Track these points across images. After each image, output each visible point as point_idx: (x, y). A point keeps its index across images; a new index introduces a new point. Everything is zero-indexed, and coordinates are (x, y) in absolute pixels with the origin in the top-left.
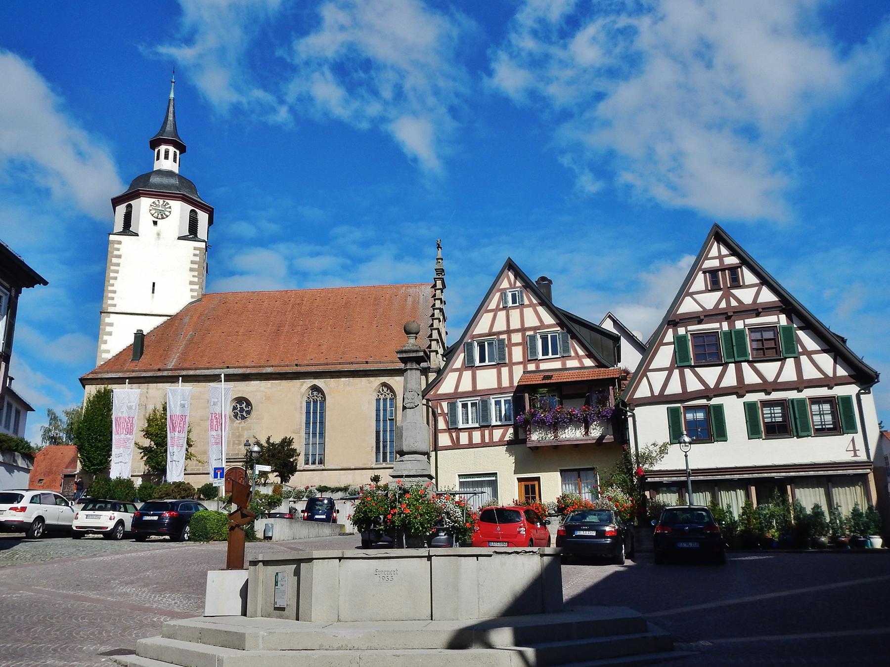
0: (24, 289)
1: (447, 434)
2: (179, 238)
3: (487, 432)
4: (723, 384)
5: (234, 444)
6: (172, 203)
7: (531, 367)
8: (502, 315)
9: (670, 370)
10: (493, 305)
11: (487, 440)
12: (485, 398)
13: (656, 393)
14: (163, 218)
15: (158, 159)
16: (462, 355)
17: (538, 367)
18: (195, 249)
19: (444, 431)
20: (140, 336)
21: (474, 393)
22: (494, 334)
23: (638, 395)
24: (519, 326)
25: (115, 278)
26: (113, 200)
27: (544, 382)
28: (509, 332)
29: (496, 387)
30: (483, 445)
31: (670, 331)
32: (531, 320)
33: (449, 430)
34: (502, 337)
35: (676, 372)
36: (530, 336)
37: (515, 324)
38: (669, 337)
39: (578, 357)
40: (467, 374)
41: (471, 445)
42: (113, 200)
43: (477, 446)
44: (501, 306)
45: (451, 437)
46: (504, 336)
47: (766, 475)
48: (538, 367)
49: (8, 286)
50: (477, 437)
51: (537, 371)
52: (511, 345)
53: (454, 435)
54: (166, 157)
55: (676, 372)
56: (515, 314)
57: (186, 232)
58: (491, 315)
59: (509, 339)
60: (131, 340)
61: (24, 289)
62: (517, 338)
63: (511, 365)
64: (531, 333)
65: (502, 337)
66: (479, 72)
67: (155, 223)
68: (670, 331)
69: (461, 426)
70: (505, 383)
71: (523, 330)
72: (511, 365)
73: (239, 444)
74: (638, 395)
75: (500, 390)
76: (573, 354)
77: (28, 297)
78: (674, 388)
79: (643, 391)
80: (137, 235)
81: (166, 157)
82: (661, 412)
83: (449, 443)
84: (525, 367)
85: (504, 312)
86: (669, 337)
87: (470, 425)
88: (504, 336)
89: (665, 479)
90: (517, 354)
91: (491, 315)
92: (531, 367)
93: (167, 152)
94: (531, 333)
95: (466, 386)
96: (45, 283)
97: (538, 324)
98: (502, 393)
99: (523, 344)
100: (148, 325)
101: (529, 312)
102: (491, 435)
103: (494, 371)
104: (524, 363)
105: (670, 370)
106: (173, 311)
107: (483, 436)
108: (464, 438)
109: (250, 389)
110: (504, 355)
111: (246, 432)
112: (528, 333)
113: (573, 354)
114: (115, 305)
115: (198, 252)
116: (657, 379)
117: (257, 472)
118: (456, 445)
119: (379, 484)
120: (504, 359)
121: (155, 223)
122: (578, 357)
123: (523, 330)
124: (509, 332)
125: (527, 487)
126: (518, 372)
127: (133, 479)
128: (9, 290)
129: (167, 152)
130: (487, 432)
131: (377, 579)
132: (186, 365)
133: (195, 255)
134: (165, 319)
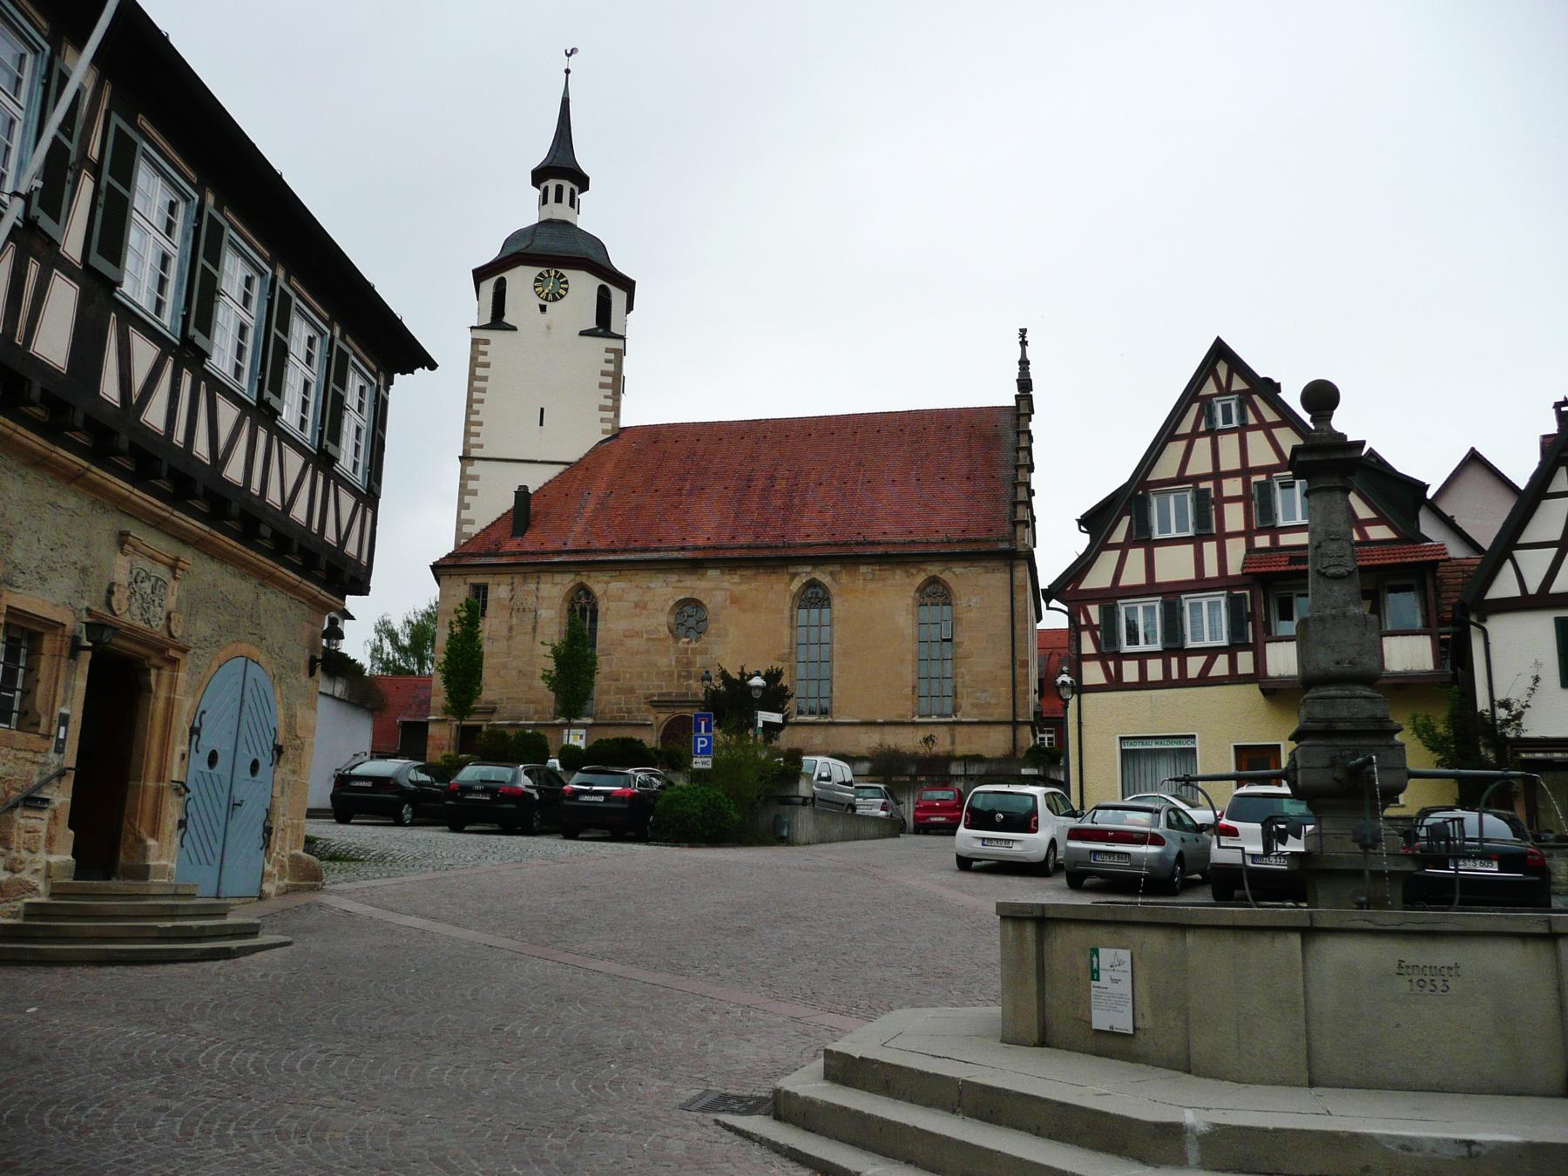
0: (397, 376)
1: (1098, 664)
2: (582, 333)
3: (1174, 661)
5: (679, 676)
6: (569, 274)
7: (1262, 541)
8: (1203, 445)
10: (1186, 427)
11: (1175, 675)
12: (1171, 598)
13: (1533, 588)
14: (555, 299)
16: (1126, 520)
17: (1274, 541)
18: (608, 350)
20: (522, 494)
21: (1150, 588)
23: (1495, 592)
24: (1237, 465)
25: (481, 401)
26: (475, 272)
27: (1293, 568)
28: (1218, 476)
29: (1193, 577)
30: (1167, 683)
33: (1101, 657)
34: (1203, 485)
36: (1258, 483)
40: (1136, 556)
41: (1143, 684)
42: (475, 272)
43: (1156, 685)
44: (1202, 428)
45: (1106, 669)
46: (1209, 485)
47: (1539, 755)
48: (1274, 541)
49: (374, 367)
50: (1221, 667)
51: (1275, 547)
52: (1221, 500)
53: (1111, 664)
54: (559, 199)
56: (1229, 444)
57: (592, 324)
58: (1182, 444)
59: (1219, 489)
60: (509, 503)
61: (397, 376)
62: (1233, 487)
63: (1221, 537)
64: (1262, 478)
65: (1203, 485)
67: (543, 308)
69: (1189, 644)
70: (1211, 570)
71: (1245, 472)
72: (1221, 537)
73: (688, 677)
74: (1495, 592)
75: (1201, 584)
77: (405, 388)
79: (1504, 586)
80: (514, 329)
81: (559, 199)
83: (1103, 680)
85: (1207, 441)
87: (1142, 647)
88: (1209, 485)
90: (1234, 517)
91: (1182, 444)
92: (1262, 541)
93: (559, 189)
94: (1262, 478)
95: (1134, 574)
96: (433, 366)
99: (1246, 498)
100: (534, 479)
102: (1183, 667)
103: (1189, 549)
104: (1248, 534)
106: (574, 457)
107: (1167, 669)
108: (1130, 672)
109: (713, 587)
110: (1209, 518)
111: (698, 658)
112: (1255, 479)
114: (481, 446)
116: (1534, 565)
117: (760, 724)
118: (1115, 683)
120: (1209, 526)
121: (543, 308)
123: (1245, 472)
124: (1218, 476)
126: (1236, 552)
127: (542, 732)
128: (376, 376)
129: (559, 189)
130: (1174, 661)
131: (1403, 985)
132: (596, 544)
133: (607, 361)
134: (561, 468)
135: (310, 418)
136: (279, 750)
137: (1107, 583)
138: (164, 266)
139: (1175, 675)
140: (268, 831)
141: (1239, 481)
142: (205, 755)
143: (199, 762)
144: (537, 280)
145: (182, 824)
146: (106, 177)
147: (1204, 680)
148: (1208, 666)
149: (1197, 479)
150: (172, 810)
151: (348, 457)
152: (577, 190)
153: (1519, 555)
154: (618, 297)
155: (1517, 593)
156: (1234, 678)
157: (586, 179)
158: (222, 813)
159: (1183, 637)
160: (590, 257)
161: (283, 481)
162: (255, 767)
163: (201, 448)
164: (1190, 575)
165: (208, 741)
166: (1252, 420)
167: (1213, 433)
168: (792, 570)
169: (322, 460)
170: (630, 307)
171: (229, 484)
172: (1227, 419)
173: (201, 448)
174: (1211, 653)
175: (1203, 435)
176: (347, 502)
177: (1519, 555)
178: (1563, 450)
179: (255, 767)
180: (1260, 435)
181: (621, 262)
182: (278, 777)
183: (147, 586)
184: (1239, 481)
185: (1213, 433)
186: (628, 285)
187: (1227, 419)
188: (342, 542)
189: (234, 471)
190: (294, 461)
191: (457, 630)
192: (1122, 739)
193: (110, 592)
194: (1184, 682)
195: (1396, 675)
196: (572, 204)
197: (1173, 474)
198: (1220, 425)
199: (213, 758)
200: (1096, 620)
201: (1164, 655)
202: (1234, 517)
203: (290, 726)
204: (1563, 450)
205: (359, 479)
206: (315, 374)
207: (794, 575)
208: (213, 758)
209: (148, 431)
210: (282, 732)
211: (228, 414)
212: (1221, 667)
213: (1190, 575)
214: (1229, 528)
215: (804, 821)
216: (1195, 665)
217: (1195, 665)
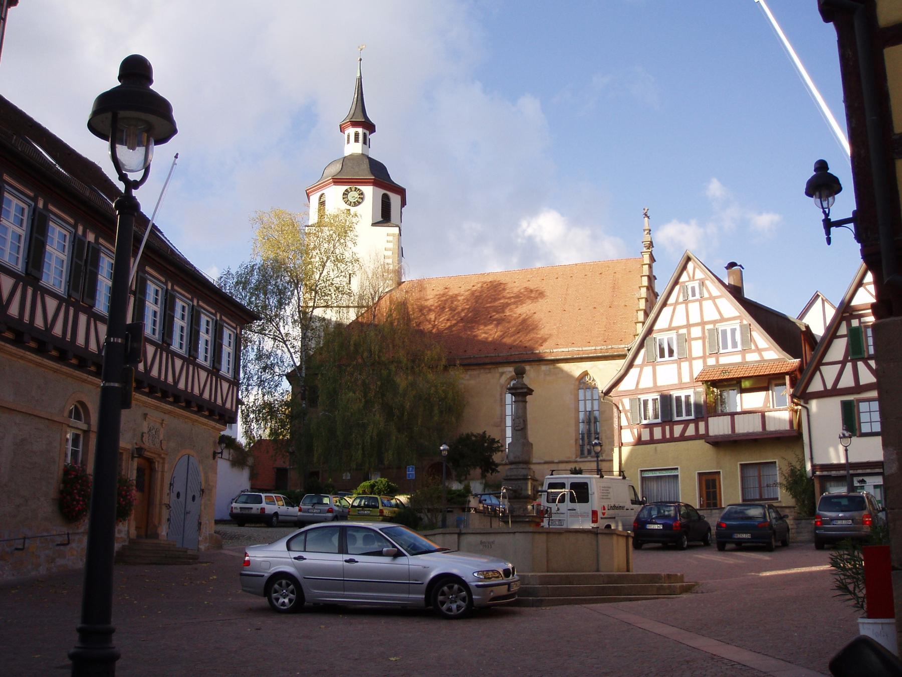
3: (667, 428)
4: (841, 385)
7: (711, 361)
8: (681, 308)
9: (843, 363)
10: (672, 300)
11: (668, 436)
13: (829, 387)
15: (348, 142)
19: (627, 427)
22: (674, 329)
30: (664, 440)
31: (844, 324)
32: (710, 314)
35: (849, 365)
37: (695, 318)
38: (843, 330)
39: (759, 350)
55: (849, 365)
59: (689, 333)
62: (696, 332)
63: (690, 359)
66: (117, 546)
68: (844, 324)
70: (686, 379)
71: (703, 323)
76: (753, 347)
78: (847, 381)
82: (834, 405)
84: (705, 362)
85: (684, 305)
86: (843, 330)
87: (684, 417)
89: (834, 473)
90: (697, 348)
93: (357, 135)
94: (711, 326)
97: (718, 317)
98: (682, 388)
101: (708, 305)
105: (843, 363)
112: (708, 327)
113: (753, 347)
115: (391, 238)
116: (829, 373)
119: (287, 465)
122: (759, 350)
123: (703, 323)
124: (688, 326)
125: (707, 482)
130: (667, 428)
135: (209, 355)
136: (203, 491)
137: (633, 387)
138: (155, 316)
139: (668, 436)
140: (200, 524)
141: (700, 328)
142: (176, 493)
143: (173, 496)
144: (344, 194)
145: (169, 520)
146: (138, 295)
147: (683, 438)
148: (684, 430)
149: (677, 328)
150: (165, 513)
151: (225, 369)
152: (367, 132)
153: (823, 368)
154: (395, 199)
155: (821, 388)
156: (697, 437)
157: (374, 126)
158: (182, 517)
159: (672, 415)
160: (379, 175)
161: (198, 383)
162: (194, 498)
163: (170, 379)
164: (676, 382)
165: (176, 489)
166: (706, 295)
167: (686, 301)
168: (501, 370)
169: (214, 371)
170: (404, 203)
171: (181, 390)
172: (694, 295)
173: (170, 379)
174: (686, 423)
175: (681, 303)
176: (225, 385)
177: (823, 368)
178: (843, 312)
179: (194, 498)
180: (710, 302)
181: (396, 177)
182: (203, 502)
183: (153, 432)
184: (700, 328)
185: (686, 301)
186: (401, 191)
187: (694, 295)
188: (224, 403)
189: (181, 385)
190: (203, 375)
191: (434, 331)
192: (642, 471)
193: (142, 436)
194: (673, 439)
195: (772, 432)
196: (365, 142)
197: (666, 326)
198: (690, 298)
199: (178, 495)
200: (628, 407)
201: (662, 424)
202: (697, 348)
203: (207, 481)
204: (843, 312)
205: (230, 376)
206: (209, 337)
207: (502, 373)
208: (178, 495)
209: (153, 378)
210: (203, 483)
211: (178, 363)
212: (691, 431)
213: (676, 382)
214: (694, 355)
215: (475, 521)
216: (678, 430)
217: (678, 430)
